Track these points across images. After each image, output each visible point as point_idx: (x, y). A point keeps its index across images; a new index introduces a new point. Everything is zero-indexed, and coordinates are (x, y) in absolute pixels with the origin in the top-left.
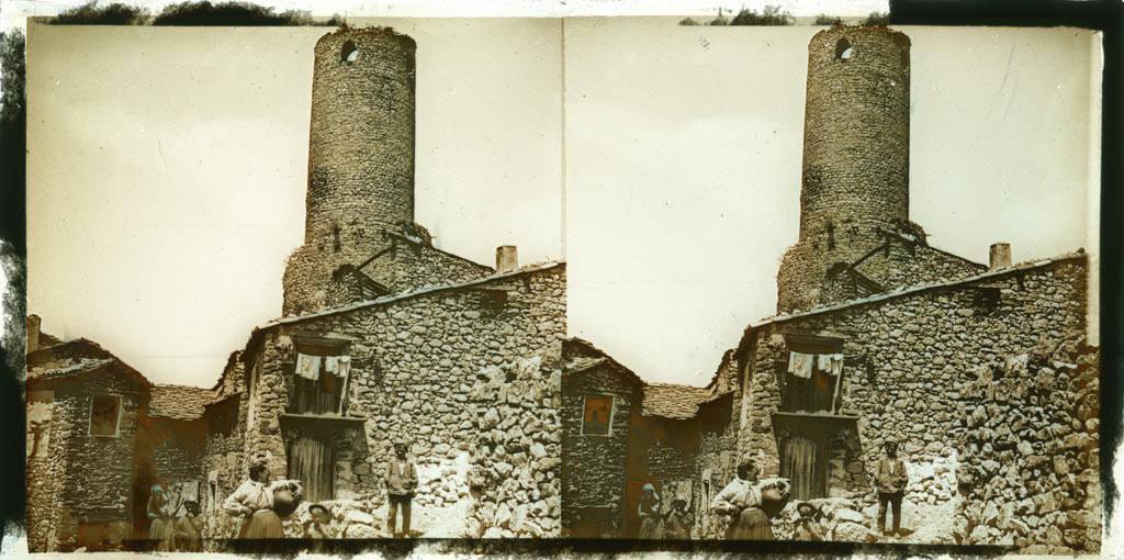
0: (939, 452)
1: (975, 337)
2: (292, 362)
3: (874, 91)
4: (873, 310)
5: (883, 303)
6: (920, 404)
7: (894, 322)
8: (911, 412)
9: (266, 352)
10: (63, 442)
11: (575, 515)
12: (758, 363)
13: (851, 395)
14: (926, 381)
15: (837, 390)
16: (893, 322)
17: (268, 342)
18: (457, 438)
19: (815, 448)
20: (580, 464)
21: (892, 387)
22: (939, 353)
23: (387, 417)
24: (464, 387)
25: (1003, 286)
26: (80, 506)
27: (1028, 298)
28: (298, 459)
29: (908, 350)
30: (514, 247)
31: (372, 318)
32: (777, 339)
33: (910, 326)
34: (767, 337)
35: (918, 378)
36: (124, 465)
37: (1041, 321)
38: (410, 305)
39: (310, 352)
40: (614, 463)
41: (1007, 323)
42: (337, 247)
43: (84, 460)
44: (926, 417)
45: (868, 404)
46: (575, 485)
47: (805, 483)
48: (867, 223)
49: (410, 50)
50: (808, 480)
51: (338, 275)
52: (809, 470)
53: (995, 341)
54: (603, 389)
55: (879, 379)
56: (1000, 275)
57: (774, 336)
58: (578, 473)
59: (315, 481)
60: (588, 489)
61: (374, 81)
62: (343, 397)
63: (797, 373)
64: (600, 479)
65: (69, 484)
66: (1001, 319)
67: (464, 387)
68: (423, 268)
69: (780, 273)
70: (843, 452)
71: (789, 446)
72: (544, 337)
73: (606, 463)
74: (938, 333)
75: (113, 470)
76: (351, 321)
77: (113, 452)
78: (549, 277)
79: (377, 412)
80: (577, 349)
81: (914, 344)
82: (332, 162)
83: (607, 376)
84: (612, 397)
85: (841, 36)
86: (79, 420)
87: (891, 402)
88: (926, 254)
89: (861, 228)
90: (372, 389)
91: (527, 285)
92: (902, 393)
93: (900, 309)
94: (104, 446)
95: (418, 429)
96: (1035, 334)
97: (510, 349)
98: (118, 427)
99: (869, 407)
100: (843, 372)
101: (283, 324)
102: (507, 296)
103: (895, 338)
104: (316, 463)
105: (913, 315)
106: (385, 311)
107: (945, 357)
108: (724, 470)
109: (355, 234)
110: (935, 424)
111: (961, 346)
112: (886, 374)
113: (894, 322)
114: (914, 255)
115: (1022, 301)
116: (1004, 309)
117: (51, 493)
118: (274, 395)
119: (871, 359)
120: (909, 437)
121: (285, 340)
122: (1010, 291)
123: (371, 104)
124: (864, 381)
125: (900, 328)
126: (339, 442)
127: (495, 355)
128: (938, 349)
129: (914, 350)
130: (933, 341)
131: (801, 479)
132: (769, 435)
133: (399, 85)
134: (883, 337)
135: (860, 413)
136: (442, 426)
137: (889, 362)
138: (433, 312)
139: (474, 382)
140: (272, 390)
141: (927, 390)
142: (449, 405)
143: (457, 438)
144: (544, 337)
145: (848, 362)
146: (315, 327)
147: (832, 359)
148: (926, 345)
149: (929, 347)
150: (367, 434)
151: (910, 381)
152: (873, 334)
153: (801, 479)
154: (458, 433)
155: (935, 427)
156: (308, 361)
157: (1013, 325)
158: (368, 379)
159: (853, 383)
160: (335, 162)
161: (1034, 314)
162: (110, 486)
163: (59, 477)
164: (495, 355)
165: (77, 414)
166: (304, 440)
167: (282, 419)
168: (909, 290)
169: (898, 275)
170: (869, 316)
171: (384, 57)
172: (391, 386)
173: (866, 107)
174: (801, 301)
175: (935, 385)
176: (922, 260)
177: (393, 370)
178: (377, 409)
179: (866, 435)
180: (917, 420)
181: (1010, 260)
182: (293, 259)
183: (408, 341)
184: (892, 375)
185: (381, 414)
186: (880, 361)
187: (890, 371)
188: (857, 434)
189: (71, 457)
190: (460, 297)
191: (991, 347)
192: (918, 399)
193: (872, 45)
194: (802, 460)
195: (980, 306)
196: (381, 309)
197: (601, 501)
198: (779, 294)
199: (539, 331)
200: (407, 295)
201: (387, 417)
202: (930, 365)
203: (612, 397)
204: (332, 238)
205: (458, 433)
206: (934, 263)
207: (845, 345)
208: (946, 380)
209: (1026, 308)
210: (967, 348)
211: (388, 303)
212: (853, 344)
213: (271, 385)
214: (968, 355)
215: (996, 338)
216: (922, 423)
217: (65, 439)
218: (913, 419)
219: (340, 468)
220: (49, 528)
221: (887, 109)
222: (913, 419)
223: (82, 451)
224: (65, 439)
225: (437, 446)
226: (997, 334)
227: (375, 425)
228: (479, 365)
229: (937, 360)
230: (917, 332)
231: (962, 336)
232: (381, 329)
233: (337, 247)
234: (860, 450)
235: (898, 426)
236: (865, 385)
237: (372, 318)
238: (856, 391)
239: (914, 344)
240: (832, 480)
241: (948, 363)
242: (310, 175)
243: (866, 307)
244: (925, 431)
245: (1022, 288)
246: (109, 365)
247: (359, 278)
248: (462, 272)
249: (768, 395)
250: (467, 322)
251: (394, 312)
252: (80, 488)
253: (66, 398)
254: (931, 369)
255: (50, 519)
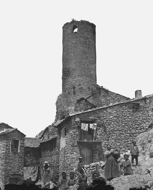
1: (133, 118)
2: (80, 126)
4: (105, 110)
5: (107, 108)
6: (119, 137)
7: (110, 114)
10: (2, 154)
12: (72, 127)
13: (99, 135)
14: (120, 131)
16: (110, 114)
17: (73, 120)
18: (127, 146)
21: (111, 133)
24: (129, 132)
25: (141, 103)
26: (10, 173)
27: (147, 106)
28: (83, 154)
31: (102, 112)
34: (75, 119)
35: (118, 130)
36: (22, 161)
37: (151, 113)
38: (113, 108)
39: (86, 122)
41: (142, 113)
43: (10, 160)
44: (120, 141)
46: (10, 167)
47: (87, 161)
48: (85, 86)
49: (94, 29)
50: (88, 160)
51: (79, 101)
53: (139, 119)
54: (16, 138)
55: (107, 131)
57: (77, 119)
59: (88, 159)
60: (14, 168)
61: (84, 39)
62: (94, 136)
63: (84, 129)
64: (17, 165)
65: (6, 167)
67: (129, 132)
68: (109, 98)
69: (57, 102)
71: (82, 151)
74: (123, 117)
76: (96, 113)
77: (18, 157)
80: (4, 126)
81: (116, 120)
84: (19, 140)
85: (74, 25)
86: (8, 147)
88: (111, 94)
91: (145, 102)
92: (114, 135)
93: (112, 110)
94: (15, 155)
95: (117, 144)
96: (150, 117)
97: (141, 120)
99: (105, 139)
100: (96, 128)
101: (77, 114)
103: (111, 118)
104: (88, 155)
105: (116, 111)
106: (106, 110)
107: (125, 124)
108: (54, 161)
109: (80, 89)
110: (123, 143)
112: (109, 129)
113: (110, 114)
115: (146, 107)
116: (141, 109)
118: (75, 136)
121: (78, 119)
122: (142, 104)
123: (83, 46)
124: (103, 131)
129: (116, 122)
131: (86, 160)
132: (77, 148)
133: (91, 40)
134: (108, 118)
138: (119, 110)
139: (131, 130)
140: (75, 134)
141: (120, 134)
142: (125, 137)
143: (127, 146)
145: (98, 126)
147: (94, 125)
148: (120, 120)
150: (102, 146)
151: (116, 131)
152: (105, 117)
153: (86, 160)
154: (128, 145)
155: (123, 144)
158: (102, 130)
159: (100, 132)
160: (72, 66)
161: (149, 111)
162: (18, 167)
165: (7, 146)
166: (84, 149)
167: (78, 143)
168: (114, 104)
169: (104, 101)
170: (103, 112)
171: (87, 31)
173: (83, 48)
175: (123, 132)
177: (109, 127)
178: (105, 139)
179: (104, 147)
181: (141, 95)
182: (60, 97)
184: (110, 129)
185: (106, 140)
187: (110, 128)
189: (6, 159)
190: (127, 105)
191: (138, 121)
192: (118, 136)
193: (84, 28)
194: (86, 154)
195: (134, 109)
196: (105, 109)
197: (17, 172)
199: (149, 115)
200: (111, 105)
201: (108, 141)
202: (121, 126)
203: (19, 140)
204: (73, 90)
205: (128, 145)
206: (114, 97)
208: (126, 130)
209: (147, 109)
210: (131, 121)
212: (99, 120)
213: (74, 133)
219: (95, 156)
222: (117, 142)
223: (9, 157)
224: (3, 153)
225: (122, 149)
226: (139, 117)
228: (133, 125)
232: (105, 115)
233: (74, 93)
234: (103, 151)
235: (113, 144)
236: (103, 132)
237: (102, 112)
238: (101, 134)
239: (116, 120)
243: (102, 109)
245: (146, 103)
246: (13, 132)
248: (120, 99)
249: (76, 136)
250: (129, 113)
251: (108, 110)
252: (9, 168)
254: (121, 127)
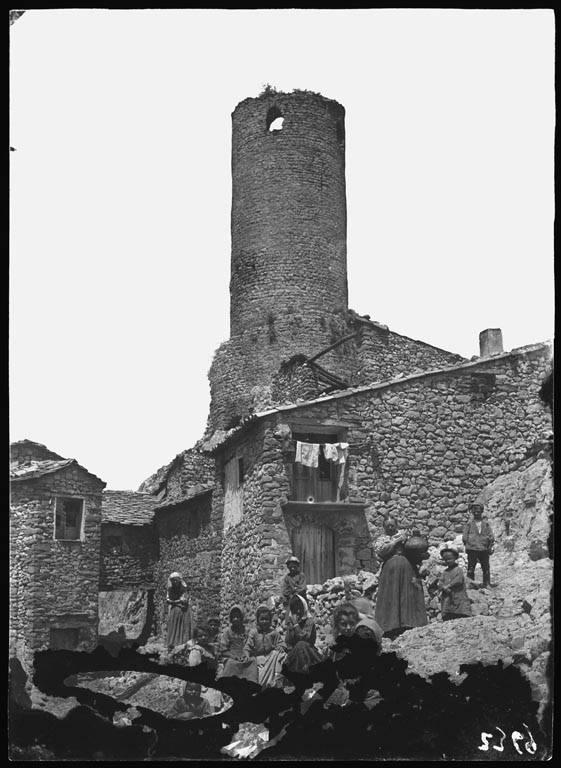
0: (443, 537)
2: (293, 450)
3: (310, 167)
4: (376, 398)
5: (384, 389)
6: (424, 490)
8: (415, 498)
9: (265, 441)
10: (27, 548)
11: (54, 622)
12: (265, 454)
13: (356, 482)
14: (428, 468)
15: (342, 479)
16: (394, 409)
17: (266, 431)
18: (453, 521)
19: (324, 537)
20: (54, 571)
21: (396, 474)
22: (440, 439)
24: (458, 471)
26: (51, 613)
27: (522, 384)
29: (410, 438)
30: (499, 330)
33: (410, 413)
34: (273, 428)
37: (534, 406)
39: (311, 438)
40: (88, 569)
41: (502, 409)
42: (272, 339)
43: (52, 566)
44: (429, 503)
45: (374, 492)
47: (315, 572)
51: (287, 368)
52: (318, 557)
54: (73, 492)
55: (384, 467)
56: (495, 361)
57: (280, 426)
58: (54, 580)
61: (304, 153)
62: (341, 484)
63: (304, 462)
66: (497, 405)
67: (458, 471)
68: (390, 356)
70: (353, 540)
71: (298, 536)
72: (531, 419)
73: (82, 569)
74: (438, 420)
75: (81, 575)
76: (347, 407)
78: (535, 360)
79: (376, 498)
80: (30, 452)
81: (416, 431)
82: (261, 244)
83: (76, 478)
84: (82, 500)
86: (44, 524)
88: (399, 343)
89: (303, 319)
90: (370, 476)
91: (514, 369)
92: (406, 481)
93: (401, 396)
95: (416, 513)
97: (500, 432)
99: (375, 495)
101: (280, 411)
102: (496, 379)
103: (397, 426)
105: (413, 402)
106: (379, 396)
109: (292, 323)
110: (439, 509)
111: (460, 432)
112: (390, 461)
114: (387, 344)
115: (517, 387)
117: (17, 602)
118: (274, 484)
119: (375, 447)
120: (415, 523)
121: (283, 429)
122: (505, 376)
124: (369, 469)
126: (341, 528)
127: (486, 438)
128: (438, 435)
130: (434, 428)
131: (312, 569)
134: (386, 424)
135: (367, 501)
136: (439, 509)
137: (393, 450)
138: (426, 396)
139: (467, 465)
140: (274, 479)
141: (430, 477)
142: (444, 489)
143: (453, 521)
144: (531, 419)
145: (352, 450)
146: (313, 414)
147: (338, 448)
149: (430, 434)
151: (413, 468)
152: (376, 422)
153: (312, 569)
155: (438, 513)
156: (307, 448)
157: (508, 411)
158: (366, 466)
160: (264, 245)
162: (79, 592)
163: (25, 585)
164: (486, 438)
167: (285, 508)
168: (409, 377)
169: (373, 366)
170: (371, 403)
171: (314, 126)
172: (388, 471)
173: (303, 185)
174: (240, 400)
175: (437, 472)
176: (395, 349)
179: (374, 523)
180: (421, 506)
181: (502, 346)
182: (222, 352)
183: (403, 426)
184: (395, 463)
187: (394, 459)
188: (365, 521)
189: (39, 563)
190: (451, 381)
191: (488, 433)
192: (422, 485)
194: (312, 548)
196: (376, 394)
198: (212, 393)
200: (399, 381)
201: (386, 502)
202: (431, 452)
203: (82, 500)
204: (266, 328)
206: (407, 352)
207: (349, 433)
208: (447, 466)
209: (520, 393)
210: (465, 435)
211: (382, 388)
213: (272, 474)
214: (467, 441)
215: (493, 423)
216: (426, 509)
217: (28, 545)
218: (417, 505)
219: (342, 554)
220: (17, 638)
221: (325, 188)
222: (417, 505)
223: (49, 556)
224: (29, 545)
226: (494, 420)
227: (374, 511)
229: (437, 447)
230: (418, 419)
231: (461, 422)
232: (376, 415)
233: (272, 339)
236: (370, 473)
238: (362, 479)
239: (416, 431)
240: (343, 568)
241: (448, 449)
242: (234, 260)
243: (368, 395)
244: (429, 517)
245: (516, 373)
246: (63, 470)
247: (314, 370)
249: (278, 485)
250: (458, 406)
251: (389, 397)
252: (49, 595)
253: (26, 502)
254: (433, 455)
255: (17, 629)
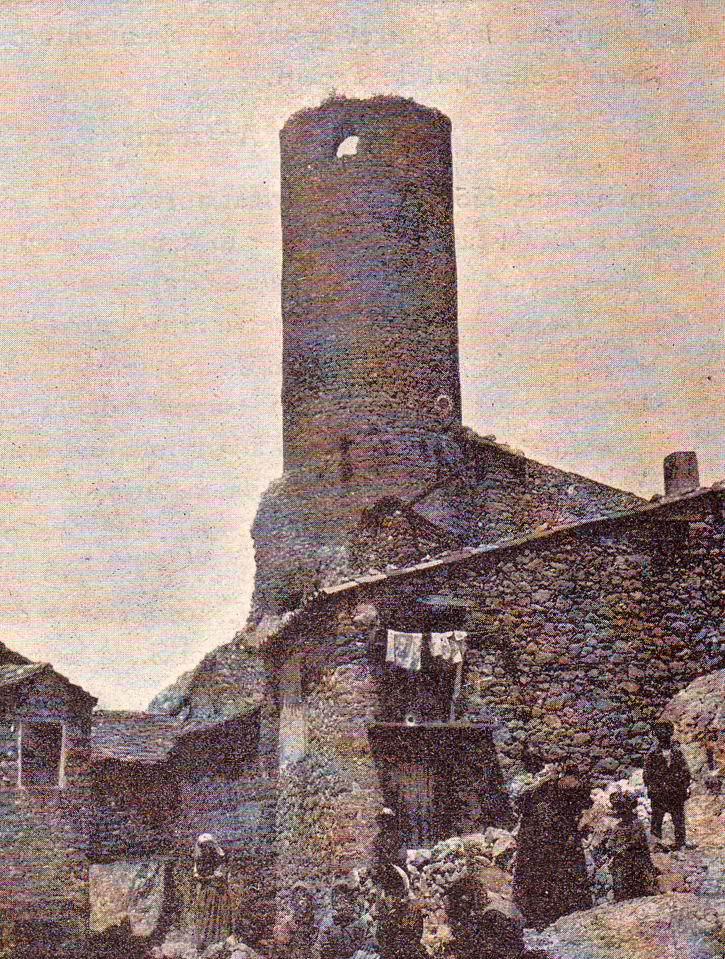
23: (525, 722)
29: (560, 621)
32: (366, 611)
54: (46, 713)
87: (540, 701)
98: (62, 772)
112: (530, 658)
122: (703, 525)
125: (545, 588)
145: (472, 642)
186: (521, 638)
191: (678, 611)
201: (525, 722)
234: (500, 776)
254: (594, 648)
